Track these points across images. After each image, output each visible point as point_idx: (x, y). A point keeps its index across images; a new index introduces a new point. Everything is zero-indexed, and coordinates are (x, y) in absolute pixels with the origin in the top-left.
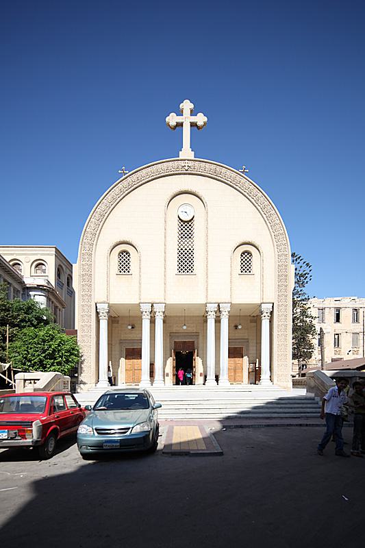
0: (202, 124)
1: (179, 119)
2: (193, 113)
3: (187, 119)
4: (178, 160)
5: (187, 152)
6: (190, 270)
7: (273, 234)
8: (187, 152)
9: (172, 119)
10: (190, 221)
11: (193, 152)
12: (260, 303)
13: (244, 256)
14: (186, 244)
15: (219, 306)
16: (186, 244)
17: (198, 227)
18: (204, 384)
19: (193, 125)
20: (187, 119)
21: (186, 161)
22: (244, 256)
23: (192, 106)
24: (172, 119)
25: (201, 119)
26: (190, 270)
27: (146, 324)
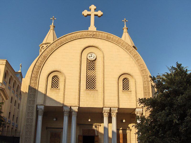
0: (99, 11)
1: (89, 13)
2: (96, 10)
3: (93, 13)
4: (88, 31)
5: (92, 28)
6: (127, 88)
7: (128, 52)
8: (92, 28)
9: (85, 13)
10: (94, 61)
11: (96, 28)
12: (135, 108)
13: (125, 81)
14: (91, 73)
15: (110, 110)
16: (91, 73)
17: (99, 65)
18: (177, 63)
19: (96, 15)
20: (93, 13)
21: (92, 32)
22: (125, 81)
23: (95, 7)
24: (85, 13)
25: (100, 13)
26: (127, 88)
27: (66, 119)
